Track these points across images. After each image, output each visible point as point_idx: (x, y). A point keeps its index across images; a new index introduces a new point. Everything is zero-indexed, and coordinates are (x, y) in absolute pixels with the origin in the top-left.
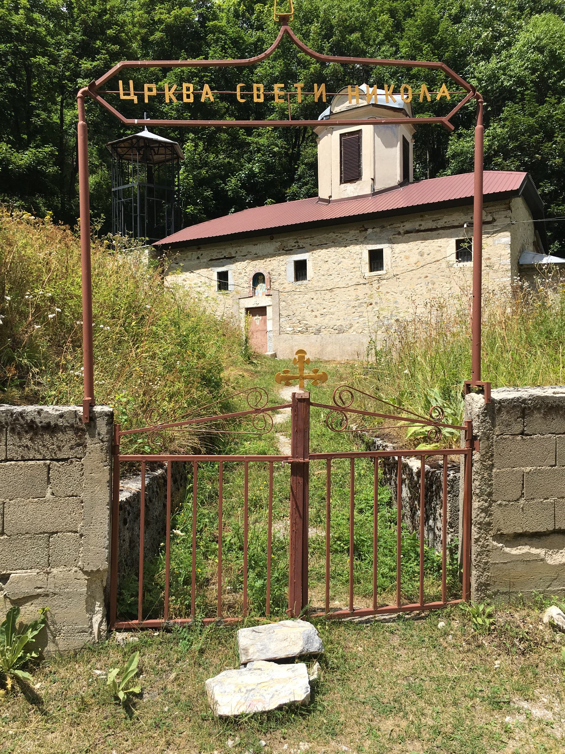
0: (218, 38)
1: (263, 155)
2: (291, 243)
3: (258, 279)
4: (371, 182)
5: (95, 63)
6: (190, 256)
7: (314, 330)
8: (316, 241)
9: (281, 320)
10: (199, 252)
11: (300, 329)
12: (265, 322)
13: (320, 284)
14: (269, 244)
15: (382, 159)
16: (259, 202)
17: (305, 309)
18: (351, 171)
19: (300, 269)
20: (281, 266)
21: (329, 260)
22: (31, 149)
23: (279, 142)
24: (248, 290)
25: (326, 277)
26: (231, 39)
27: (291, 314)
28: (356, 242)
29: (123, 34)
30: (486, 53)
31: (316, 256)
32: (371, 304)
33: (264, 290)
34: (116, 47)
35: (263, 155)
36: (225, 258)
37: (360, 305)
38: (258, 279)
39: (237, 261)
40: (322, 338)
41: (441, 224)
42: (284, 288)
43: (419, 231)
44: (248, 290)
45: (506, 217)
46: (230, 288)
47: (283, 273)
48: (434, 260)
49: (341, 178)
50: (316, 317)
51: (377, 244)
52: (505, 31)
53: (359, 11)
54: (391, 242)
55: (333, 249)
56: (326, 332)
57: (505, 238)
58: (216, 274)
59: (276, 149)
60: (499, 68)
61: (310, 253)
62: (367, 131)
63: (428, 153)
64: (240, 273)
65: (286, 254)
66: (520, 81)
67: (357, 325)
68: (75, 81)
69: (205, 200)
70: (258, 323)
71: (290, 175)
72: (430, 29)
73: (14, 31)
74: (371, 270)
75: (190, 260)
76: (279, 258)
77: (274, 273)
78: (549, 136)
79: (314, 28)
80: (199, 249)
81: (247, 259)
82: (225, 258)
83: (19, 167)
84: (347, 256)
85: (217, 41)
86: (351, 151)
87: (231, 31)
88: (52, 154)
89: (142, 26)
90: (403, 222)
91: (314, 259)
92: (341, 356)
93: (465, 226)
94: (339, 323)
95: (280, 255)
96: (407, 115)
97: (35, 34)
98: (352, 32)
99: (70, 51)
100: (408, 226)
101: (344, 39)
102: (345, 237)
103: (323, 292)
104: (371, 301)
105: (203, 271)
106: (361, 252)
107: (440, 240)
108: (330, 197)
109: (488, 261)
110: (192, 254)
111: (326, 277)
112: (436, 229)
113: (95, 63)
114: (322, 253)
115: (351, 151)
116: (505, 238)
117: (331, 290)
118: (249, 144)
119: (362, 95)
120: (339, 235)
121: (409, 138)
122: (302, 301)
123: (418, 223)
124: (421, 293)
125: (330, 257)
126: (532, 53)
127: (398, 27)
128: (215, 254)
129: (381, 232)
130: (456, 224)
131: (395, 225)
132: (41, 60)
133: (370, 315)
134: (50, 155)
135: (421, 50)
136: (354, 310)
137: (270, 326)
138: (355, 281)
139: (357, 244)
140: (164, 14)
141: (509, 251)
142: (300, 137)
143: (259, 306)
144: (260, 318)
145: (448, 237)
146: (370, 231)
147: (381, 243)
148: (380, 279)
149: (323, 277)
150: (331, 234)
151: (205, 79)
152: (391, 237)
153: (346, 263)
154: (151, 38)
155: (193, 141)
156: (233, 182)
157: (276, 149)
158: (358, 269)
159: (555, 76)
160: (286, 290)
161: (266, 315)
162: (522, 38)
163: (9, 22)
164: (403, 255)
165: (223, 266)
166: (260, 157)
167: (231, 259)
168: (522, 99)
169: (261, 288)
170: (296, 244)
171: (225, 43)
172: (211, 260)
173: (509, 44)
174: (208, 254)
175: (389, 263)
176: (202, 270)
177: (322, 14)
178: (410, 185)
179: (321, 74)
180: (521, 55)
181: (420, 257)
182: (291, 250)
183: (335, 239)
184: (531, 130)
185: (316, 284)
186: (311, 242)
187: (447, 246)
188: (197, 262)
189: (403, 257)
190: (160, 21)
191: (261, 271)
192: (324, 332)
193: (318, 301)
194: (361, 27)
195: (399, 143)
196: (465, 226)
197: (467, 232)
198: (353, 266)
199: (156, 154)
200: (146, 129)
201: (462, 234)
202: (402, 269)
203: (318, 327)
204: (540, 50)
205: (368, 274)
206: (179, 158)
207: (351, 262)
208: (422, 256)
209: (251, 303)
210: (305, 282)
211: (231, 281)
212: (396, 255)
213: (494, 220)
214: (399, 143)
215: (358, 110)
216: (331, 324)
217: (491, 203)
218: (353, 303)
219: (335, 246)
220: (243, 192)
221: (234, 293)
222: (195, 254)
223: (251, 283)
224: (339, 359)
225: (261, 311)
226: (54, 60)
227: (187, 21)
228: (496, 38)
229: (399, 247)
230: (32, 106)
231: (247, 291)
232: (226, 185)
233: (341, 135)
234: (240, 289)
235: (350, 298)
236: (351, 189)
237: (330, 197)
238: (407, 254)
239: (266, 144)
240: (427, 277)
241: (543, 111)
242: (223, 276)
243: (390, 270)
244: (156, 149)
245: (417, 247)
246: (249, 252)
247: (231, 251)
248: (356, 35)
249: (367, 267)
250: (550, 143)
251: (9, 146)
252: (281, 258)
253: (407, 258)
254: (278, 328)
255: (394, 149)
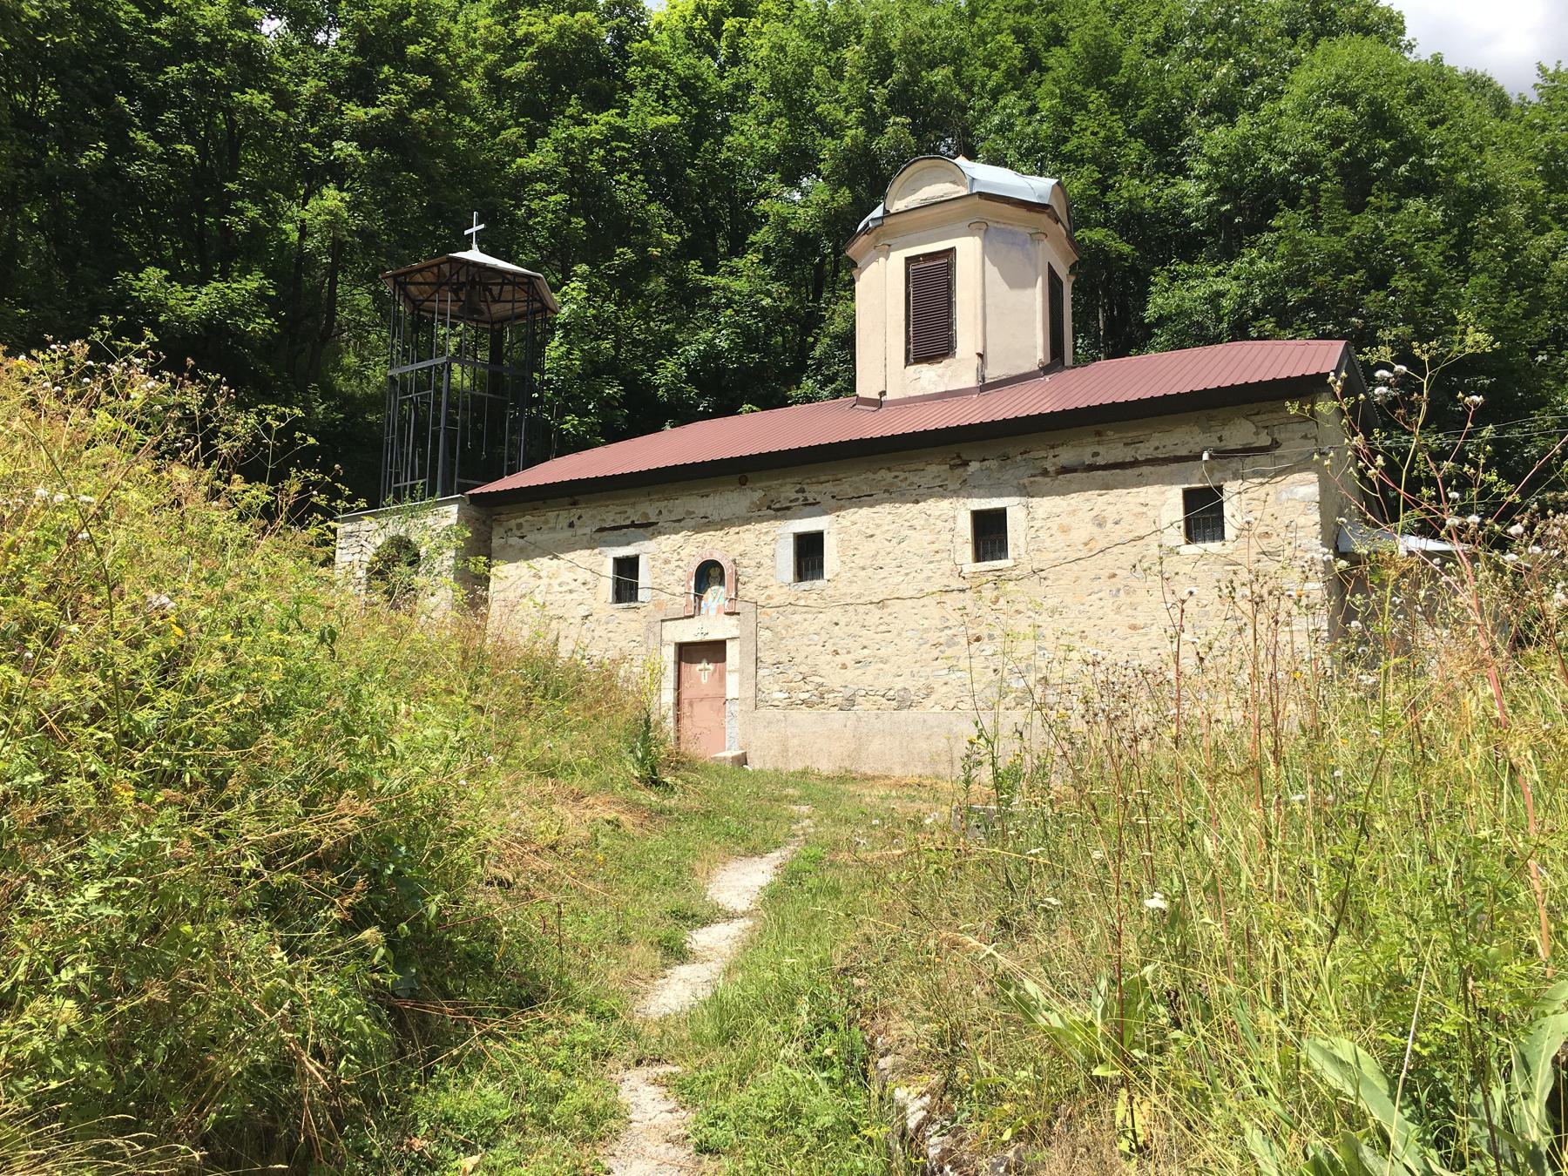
0: (650, 77)
1: (737, 313)
2: (788, 492)
3: (708, 574)
4: (977, 361)
5: (373, 112)
6: (552, 521)
7: (839, 700)
8: (846, 488)
9: (760, 672)
10: (575, 512)
11: (806, 696)
12: (722, 678)
13: (855, 589)
14: (735, 494)
15: (1004, 319)
16: (727, 408)
17: (819, 647)
18: (930, 334)
19: (809, 553)
20: (761, 548)
21: (877, 532)
22: (215, 284)
23: (774, 287)
24: (683, 601)
25: (870, 571)
26: (679, 78)
27: (785, 658)
28: (942, 491)
29: (442, 56)
30: (1225, 108)
31: (845, 522)
32: (978, 639)
33: (722, 601)
34: (425, 81)
35: (737, 313)
36: (633, 525)
37: (951, 642)
38: (708, 574)
39: (660, 533)
40: (859, 719)
41: (1144, 451)
42: (769, 597)
43: (1092, 468)
44: (683, 601)
45: (1305, 437)
46: (642, 595)
47: (767, 562)
48: (1131, 536)
49: (907, 352)
50: (844, 667)
51: (992, 496)
52: (1264, 67)
53: (951, 28)
54: (1025, 491)
55: (887, 507)
56: (868, 706)
57: (1303, 489)
58: (611, 562)
59: (767, 302)
60: (1257, 137)
61: (832, 517)
62: (968, 251)
63: (1102, 306)
64: (667, 562)
65: (776, 518)
66: (1308, 164)
67: (945, 689)
68: (330, 146)
69: (606, 404)
70: (704, 681)
71: (796, 350)
72: (1100, 65)
73: (201, 38)
74: (978, 557)
75: (553, 529)
76: (758, 526)
77: (745, 562)
78: (1380, 279)
79: (852, 54)
80: (574, 504)
81: (683, 528)
82: (633, 525)
83: (183, 319)
84: (918, 523)
85: (646, 83)
86: (931, 291)
87: (681, 65)
88: (260, 295)
89: (490, 47)
90: (1053, 447)
91: (840, 530)
92: (905, 764)
93: (1205, 456)
94: (899, 684)
95: (760, 519)
96: (1057, 220)
97: (247, 46)
98: (932, 66)
99: (322, 84)
100: (1067, 456)
101: (916, 78)
102: (916, 479)
103: (861, 609)
104: (977, 631)
105: (581, 556)
106: (953, 516)
107: (1144, 489)
108: (883, 393)
109: (1265, 541)
110: (558, 517)
111: (870, 571)
112: (1134, 464)
113: (373, 112)
114: (860, 517)
115: (931, 291)
116: (1303, 489)
117: (881, 603)
118: (707, 291)
119: (958, 177)
120: (902, 475)
121: (1062, 272)
122: (811, 630)
123: (1089, 450)
124: (1100, 613)
125: (878, 526)
126: (1328, 106)
127: (1034, 62)
128: (611, 516)
129: (1001, 468)
130: (1184, 453)
131: (1033, 454)
132: (256, 98)
133: (980, 667)
134: (257, 296)
135: (1084, 107)
136: (936, 653)
137: (732, 687)
138: (938, 583)
139: (943, 497)
140: (538, 25)
141: (1317, 518)
142: (820, 265)
143: (708, 638)
144: (711, 666)
145: (1163, 483)
146: (974, 466)
147: (1000, 495)
148: (999, 578)
149: (863, 573)
150: (883, 473)
151: (618, 154)
152: (1026, 481)
153: (919, 540)
154: (508, 72)
155: (583, 278)
156: (668, 370)
157: (767, 302)
158: (945, 555)
159: (1384, 153)
160: (773, 602)
161: (724, 660)
162: (1301, 83)
163: (193, 21)
164: (1054, 524)
165: (628, 544)
166: (730, 317)
167: (648, 528)
168: (1314, 200)
169: (715, 596)
170: (800, 495)
171: (666, 87)
172: (601, 530)
173: (1275, 93)
174: (594, 515)
175: (1022, 542)
176: (578, 552)
177: (868, 31)
178: (1067, 372)
179: (867, 150)
180: (1304, 110)
181: (1096, 530)
182: (788, 508)
183: (891, 485)
184: (1338, 264)
185: (844, 590)
186: (836, 490)
187: (1165, 502)
188: (568, 533)
189: (1055, 527)
190: (528, 39)
191: (716, 557)
192: (863, 705)
193: (850, 630)
194: (957, 57)
195: (1040, 280)
196: (1205, 456)
197: (1211, 471)
198: (935, 547)
199: (496, 301)
200: (475, 246)
201: (1198, 476)
202: (1053, 555)
203: (848, 693)
204: (1348, 100)
205: (970, 566)
206: (546, 309)
207: (930, 538)
208: (1100, 525)
209: (690, 632)
210: (818, 583)
211: (644, 578)
212: (1037, 524)
213: (1276, 444)
214: (1040, 280)
215: (947, 207)
216: (881, 685)
217: (1267, 404)
218: (933, 637)
219: (892, 501)
220: (691, 390)
221: (651, 607)
222: (565, 516)
223: (692, 583)
224: (898, 772)
225: (714, 650)
226: (284, 100)
227: (587, 40)
228: (1244, 81)
229: (1045, 505)
230: (230, 191)
231: (683, 603)
232: (655, 373)
233: (909, 260)
234: (665, 597)
235: (927, 623)
236: (930, 378)
237: (883, 393)
238: (1065, 520)
239: (746, 291)
240: (1114, 575)
241: (1361, 225)
242: (627, 569)
243: (1025, 558)
244: (496, 290)
245: (1088, 505)
246: (689, 513)
247: (647, 509)
248: (940, 74)
249: (969, 550)
250: (1382, 294)
251: (165, 272)
252: (765, 526)
253: (1065, 530)
254: (751, 693)
255: (1029, 292)
